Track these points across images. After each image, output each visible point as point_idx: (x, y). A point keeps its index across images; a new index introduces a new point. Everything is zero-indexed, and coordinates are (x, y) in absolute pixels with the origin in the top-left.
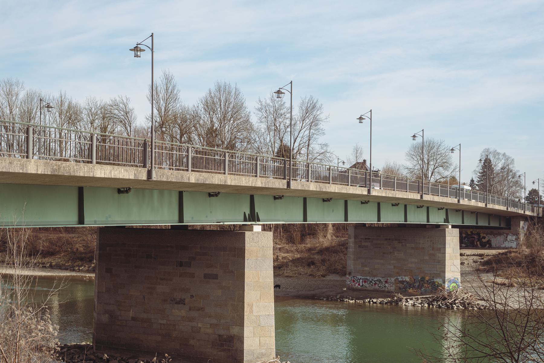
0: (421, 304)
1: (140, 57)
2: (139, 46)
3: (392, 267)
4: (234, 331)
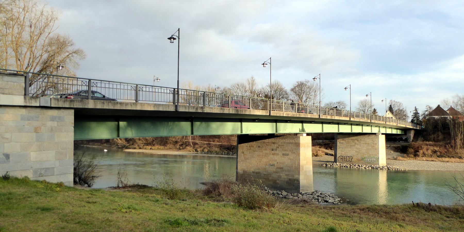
0: (368, 167)
1: (173, 42)
2: (173, 36)
3: (355, 152)
4: (296, 176)
